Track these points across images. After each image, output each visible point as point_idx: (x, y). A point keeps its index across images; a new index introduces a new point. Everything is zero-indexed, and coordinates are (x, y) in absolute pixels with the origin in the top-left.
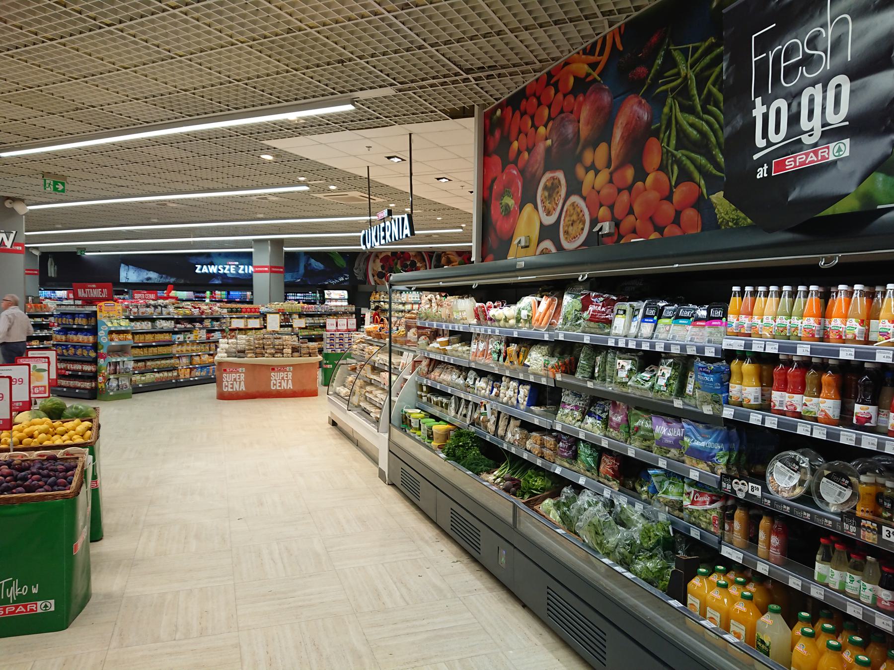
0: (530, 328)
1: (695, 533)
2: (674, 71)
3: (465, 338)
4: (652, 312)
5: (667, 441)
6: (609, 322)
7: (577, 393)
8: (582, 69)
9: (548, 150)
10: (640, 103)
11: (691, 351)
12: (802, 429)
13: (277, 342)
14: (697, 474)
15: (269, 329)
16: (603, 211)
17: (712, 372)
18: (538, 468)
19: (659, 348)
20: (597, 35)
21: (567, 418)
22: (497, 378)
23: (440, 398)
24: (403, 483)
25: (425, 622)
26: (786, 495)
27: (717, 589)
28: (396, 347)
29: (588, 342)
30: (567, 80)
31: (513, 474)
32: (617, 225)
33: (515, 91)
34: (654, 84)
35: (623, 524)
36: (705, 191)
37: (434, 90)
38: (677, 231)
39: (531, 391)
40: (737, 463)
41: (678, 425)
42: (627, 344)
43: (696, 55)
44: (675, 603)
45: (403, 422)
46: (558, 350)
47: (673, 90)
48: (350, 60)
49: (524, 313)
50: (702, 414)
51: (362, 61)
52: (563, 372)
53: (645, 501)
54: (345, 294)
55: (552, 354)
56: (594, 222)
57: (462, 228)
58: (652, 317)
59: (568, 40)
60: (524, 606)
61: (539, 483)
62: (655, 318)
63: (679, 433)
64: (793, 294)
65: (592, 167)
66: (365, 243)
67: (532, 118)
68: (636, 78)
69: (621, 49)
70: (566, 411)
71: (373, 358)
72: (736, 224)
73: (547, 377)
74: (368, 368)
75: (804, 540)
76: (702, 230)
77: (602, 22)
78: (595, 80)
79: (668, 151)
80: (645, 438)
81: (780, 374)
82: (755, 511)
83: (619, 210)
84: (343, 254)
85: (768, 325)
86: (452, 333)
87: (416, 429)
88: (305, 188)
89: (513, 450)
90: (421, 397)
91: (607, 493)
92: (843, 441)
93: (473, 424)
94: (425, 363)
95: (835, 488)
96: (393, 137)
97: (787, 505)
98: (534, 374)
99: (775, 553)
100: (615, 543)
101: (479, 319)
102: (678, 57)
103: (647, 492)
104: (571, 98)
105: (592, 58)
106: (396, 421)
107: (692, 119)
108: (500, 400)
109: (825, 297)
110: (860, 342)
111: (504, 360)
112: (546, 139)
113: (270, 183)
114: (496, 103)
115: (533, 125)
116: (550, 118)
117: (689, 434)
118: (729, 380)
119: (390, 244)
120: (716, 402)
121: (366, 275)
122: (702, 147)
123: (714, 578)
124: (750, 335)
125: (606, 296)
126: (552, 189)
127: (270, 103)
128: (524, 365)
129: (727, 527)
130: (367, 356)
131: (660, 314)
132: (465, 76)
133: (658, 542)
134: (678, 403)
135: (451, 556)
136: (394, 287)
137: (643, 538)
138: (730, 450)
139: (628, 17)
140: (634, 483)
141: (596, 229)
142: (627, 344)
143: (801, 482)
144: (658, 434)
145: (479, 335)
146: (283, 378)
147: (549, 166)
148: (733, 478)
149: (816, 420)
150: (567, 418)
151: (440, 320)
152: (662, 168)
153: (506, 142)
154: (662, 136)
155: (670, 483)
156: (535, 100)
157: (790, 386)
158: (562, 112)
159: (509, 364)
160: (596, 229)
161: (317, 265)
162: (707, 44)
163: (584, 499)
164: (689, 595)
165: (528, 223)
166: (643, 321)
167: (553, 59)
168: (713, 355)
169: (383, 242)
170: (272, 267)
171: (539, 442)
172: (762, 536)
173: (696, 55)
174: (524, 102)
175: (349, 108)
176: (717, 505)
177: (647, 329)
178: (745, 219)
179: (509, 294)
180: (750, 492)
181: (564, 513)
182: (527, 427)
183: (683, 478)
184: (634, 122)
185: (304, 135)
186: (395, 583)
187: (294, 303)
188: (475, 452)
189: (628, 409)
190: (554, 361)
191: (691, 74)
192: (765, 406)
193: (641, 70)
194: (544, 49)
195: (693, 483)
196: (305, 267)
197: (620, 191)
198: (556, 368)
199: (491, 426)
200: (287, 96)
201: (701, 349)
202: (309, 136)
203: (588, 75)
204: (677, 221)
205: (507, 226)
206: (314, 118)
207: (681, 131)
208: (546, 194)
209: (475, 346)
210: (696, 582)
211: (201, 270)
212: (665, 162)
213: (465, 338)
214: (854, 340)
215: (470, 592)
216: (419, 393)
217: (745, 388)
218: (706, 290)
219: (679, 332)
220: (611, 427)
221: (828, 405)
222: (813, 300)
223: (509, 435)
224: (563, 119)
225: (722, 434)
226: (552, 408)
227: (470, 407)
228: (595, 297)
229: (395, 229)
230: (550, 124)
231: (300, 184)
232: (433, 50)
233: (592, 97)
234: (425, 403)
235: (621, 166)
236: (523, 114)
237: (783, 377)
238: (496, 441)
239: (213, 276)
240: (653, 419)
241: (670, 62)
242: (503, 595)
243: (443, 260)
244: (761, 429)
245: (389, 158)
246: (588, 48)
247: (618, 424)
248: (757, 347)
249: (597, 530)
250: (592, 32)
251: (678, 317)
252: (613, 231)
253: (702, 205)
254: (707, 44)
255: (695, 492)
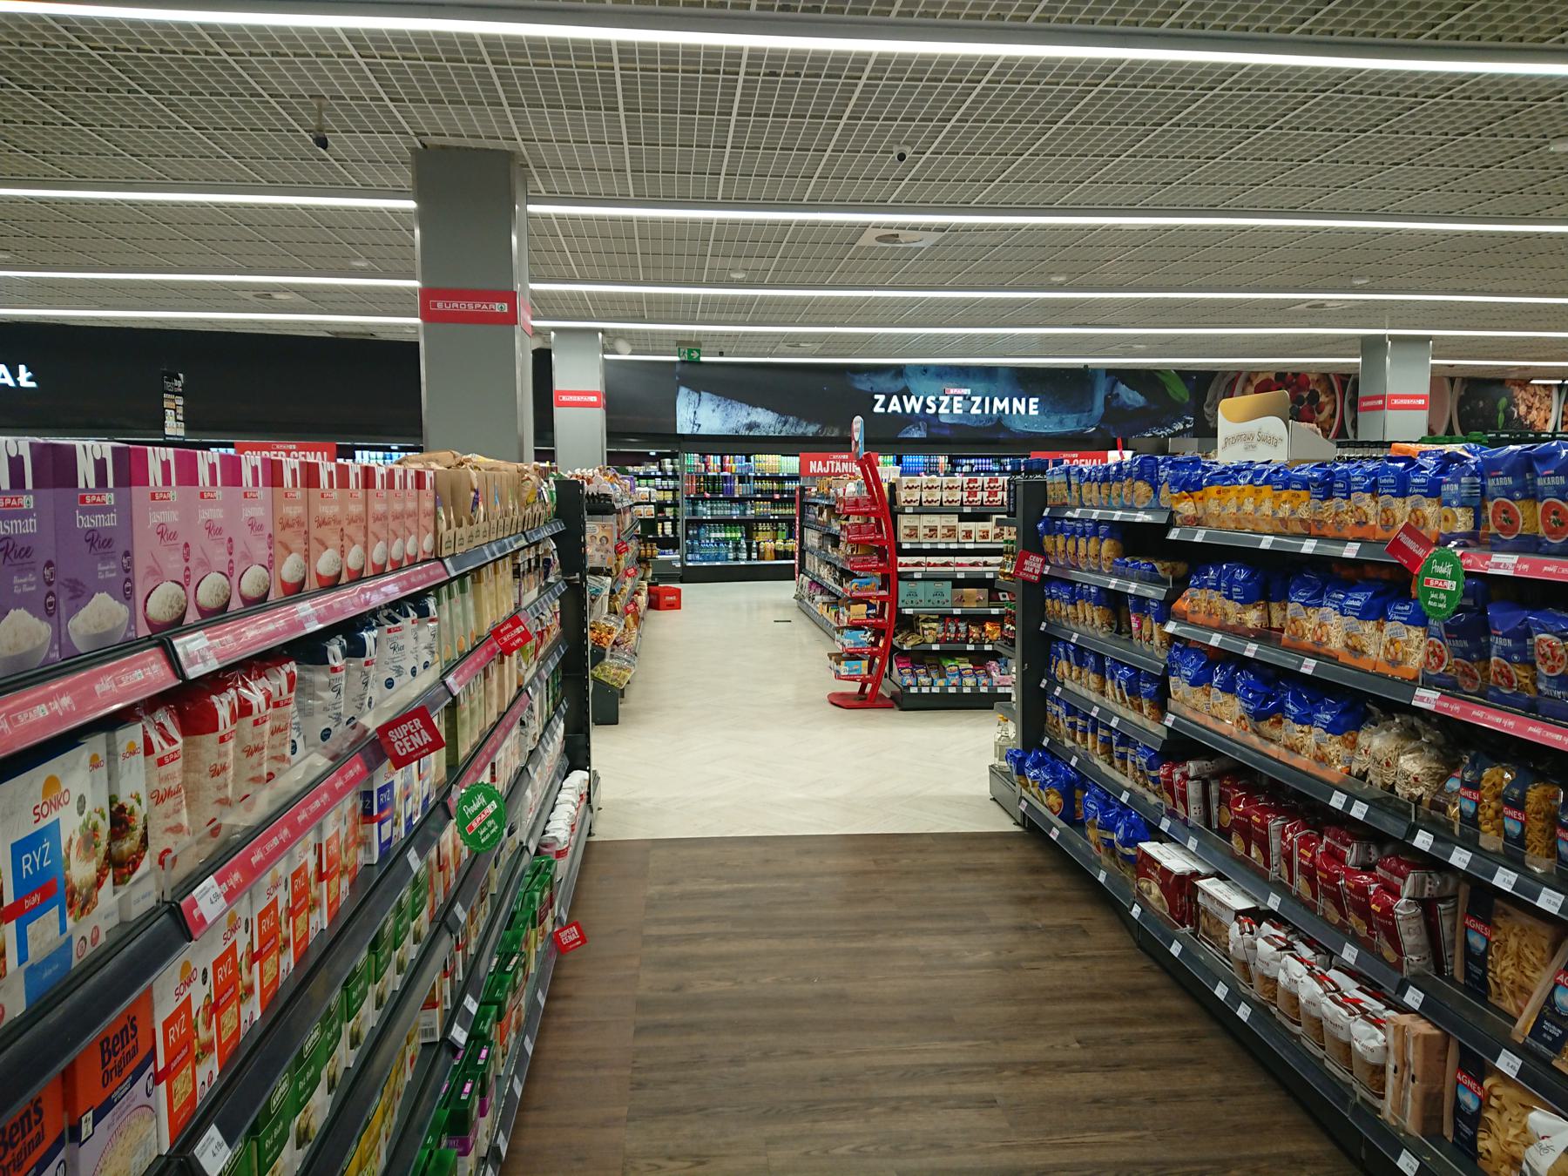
84: (1184, 375)
92: (1305, 550)
146: (409, 732)
161: (1131, 397)
170: (1382, 407)
196: (1107, 401)
211: (886, 405)
239: (907, 419)
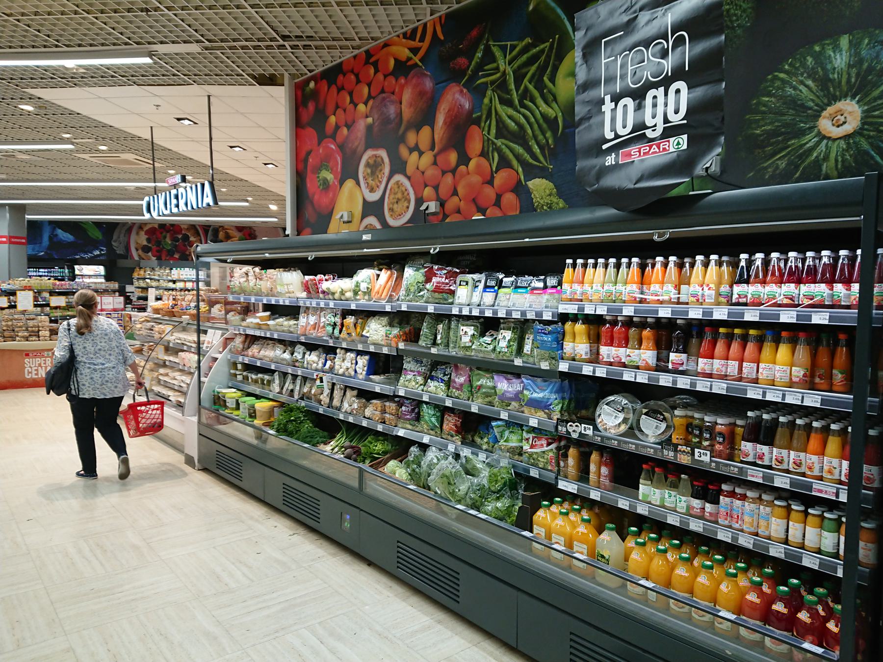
0: (370, 300)
1: (534, 473)
2: (494, 65)
3: (292, 311)
4: (493, 283)
5: (508, 395)
6: (453, 293)
7: (418, 358)
8: (404, 53)
9: (369, 128)
10: (461, 91)
11: (530, 316)
12: (628, 376)
13: (31, 323)
14: (536, 421)
15: (20, 308)
16: (428, 192)
17: (550, 333)
18: (377, 434)
19: (501, 314)
20: (418, 21)
21: (410, 383)
22: (330, 351)
23: (260, 375)
24: (219, 466)
25: (275, 595)
26: (613, 431)
27: (561, 517)
28: (204, 325)
29: (432, 311)
30: (387, 62)
31: (351, 442)
32: (442, 205)
33: (330, 65)
34: (475, 76)
35: (468, 473)
36: (522, 177)
37: (233, 53)
38: (498, 213)
39: (370, 362)
40: (568, 410)
41: (518, 381)
42: (471, 311)
43: (514, 53)
44: (526, 533)
45: (215, 403)
46: (396, 321)
47: (492, 83)
48: (156, 9)
49: (363, 287)
50: (541, 370)
51: (170, 13)
52: (404, 341)
53: (486, 450)
54: (101, 270)
55: (391, 325)
56: (419, 201)
57: (247, 201)
58: (493, 287)
59: (390, 21)
60: (370, 564)
61: (379, 447)
62: (496, 288)
63: (519, 387)
64: (618, 266)
65: (416, 148)
66: (149, 211)
67: (351, 94)
68: (457, 67)
69: (442, 38)
70: (409, 377)
71: (166, 338)
72: (550, 208)
73: (389, 346)
74: (160, 349)
75: (628, 468)
76: (520, 212)
77: (425, 9)
78: (416, 65)
79: (489, 139)
80: (487, 395)
81: (607, 333)
82: (585, 447)
83: (444, 191)
84: (98, 224)
85: (597, 292)
86: (267, 307)
87: (232, 409)
88: (71, 147)
89: (351, 419)
90: (236, 375)
91: (451, 448)
92: (662, 383)
93: (302, 398)
94: (238, 341)
95: (653, 422)
96: (189, 98)
97: (615, 440)
98: (374, 344)
99: (605, 481)
100: (466, 490)
101: (309, 292)
102: (498, 53)
103: (488, 443)
104: (392, 80)
105: (413, 43)
106: (206, 403)
107: (510, 111)
108: (336, 372)
109: (643, 267)
110: (674, 303)
111: (340, 332)
112: (367, 117)
113: (23, 138)
114: (309, 74)
115: (352, 101)
116: (370, 97)
117: (529, 387)
118: (563, 340)
119: (172, 215)
120: (553, 358)
121: (128, 248)
122: (519, 137)
123: (554, 508)
124: (581, 300)
125: (449, 268)
126: (375, 166)
127: (45, 46)
128: (362, 336)
129: (562, 464)
130: (157, 336)
131: (500, 284)
132: (281, 42)
133: (505, 484)
134: (518, 362)
135: (286, 530)
136: (202, 259)
137: (490, 481)
138: (563, 398)
139: (449, 8)
140: (473, 436)
141: (423, 208)
142: (471, 311)
143: (625, 421)
144: (500, 390)
145: (308, 308)
146: (40, 365)
147: (372, 142)
148: (567, 422)
149: (638, 368)
150: (410, 383)
151: (259, 293)
152: (484, 154)
153: (321, 116)
154: (483, 124)
155: (511, 432)
156: (353, 77)
157: (616, 342)
158: (383, 91)
159: (346, 336)
160: (423, 208)
161: (65, 236)
162: (524, 43)
163: (432, 455)
164: (535, 526)
165: (349, 201)
166: (484, 291)
167: (372, 39)
168: (550, 318)
169: (175, 210)
170: (11, 237)
171: (379, 408)
172: (593, 468)
173: (514, 53)
174: (341, 77)
175: (147, 60)
176: (553, 446)
177: (489, 297)
178: (557, 204)
179: (345, 267)
180: (583, 432)
181: (414, 470)
182: (366, 395)
183: (521, 426)
184: (456, 109)
185: (80, 86)
186: (233, 564)
187: (43, 279)
188: (307, 426)
189: (471, 370)
190: (396, 331)
191: (509, 70)
192: (595, 358)
193: (462, 61)
194: (366, 27)
195: (533, 430)
196: (50, 238)
197: (444, 173)
198: (398, 337)
199: (324, 398)
200: (70, 40)
201: (539, 314)
202: (87, 89)
203: (409, 59)
204: (498, 203)
205: (325, 201)
206: (98, 69)
207: (499, 121)
208: (369, 171)
209: (305, 320)
210: (541, 514)
212: (486, 149)
213: (292, 311)
214: (670, 302)
215: (313, 560)
216: (232, 371)
217: (577, 345)
218: (543, 261)
219: (520, 298)
220: (454, 387)
221: (648, 355)
222: (634, 268)
223: (346, 405)
224: (384, 99)
225: (557, 385)
226: (393, 376)
227: (298, 382)
228: (438, 269)
229: (192, 198)
230: (370, 103)
231: (63, 141)
232: (253, 11)
233: (414, 81)
234: (240, 382)
235: (444, 150)
236: (340, 89)
237: (609, 334)
238: (330, 412)
240: (495, 377)
241: (489, 57)
242: (346, 557)
243: (221, 235)
244: (593, 378)
245: (179, 119)
246: (409, 32)
247: (461, 385)
248: (589, 310)
249: (449, 481)
250: (413, 17)
251: (517, 287)
252: (438, 210)
253: (520, 190)
254: (524, 43)
255: (534, 438)
